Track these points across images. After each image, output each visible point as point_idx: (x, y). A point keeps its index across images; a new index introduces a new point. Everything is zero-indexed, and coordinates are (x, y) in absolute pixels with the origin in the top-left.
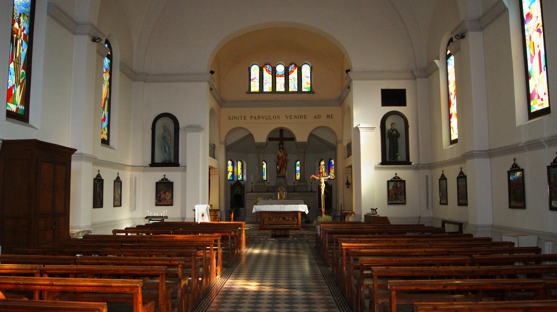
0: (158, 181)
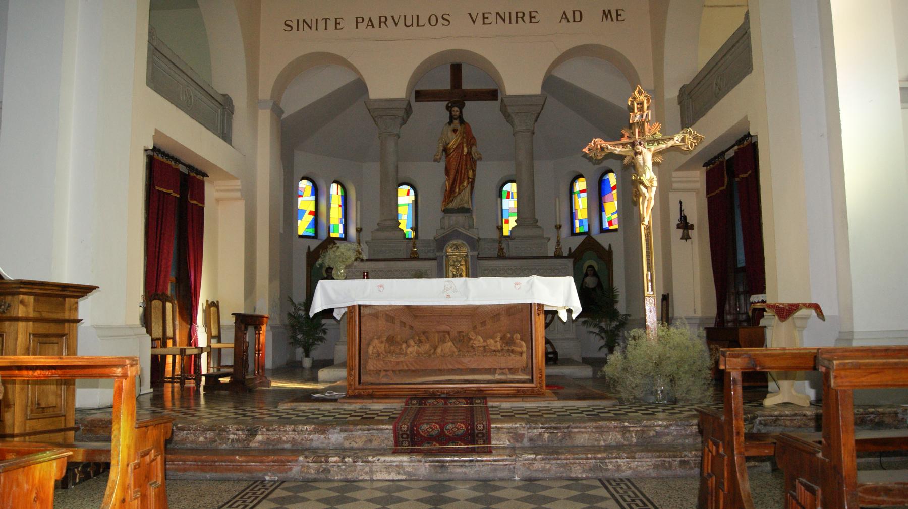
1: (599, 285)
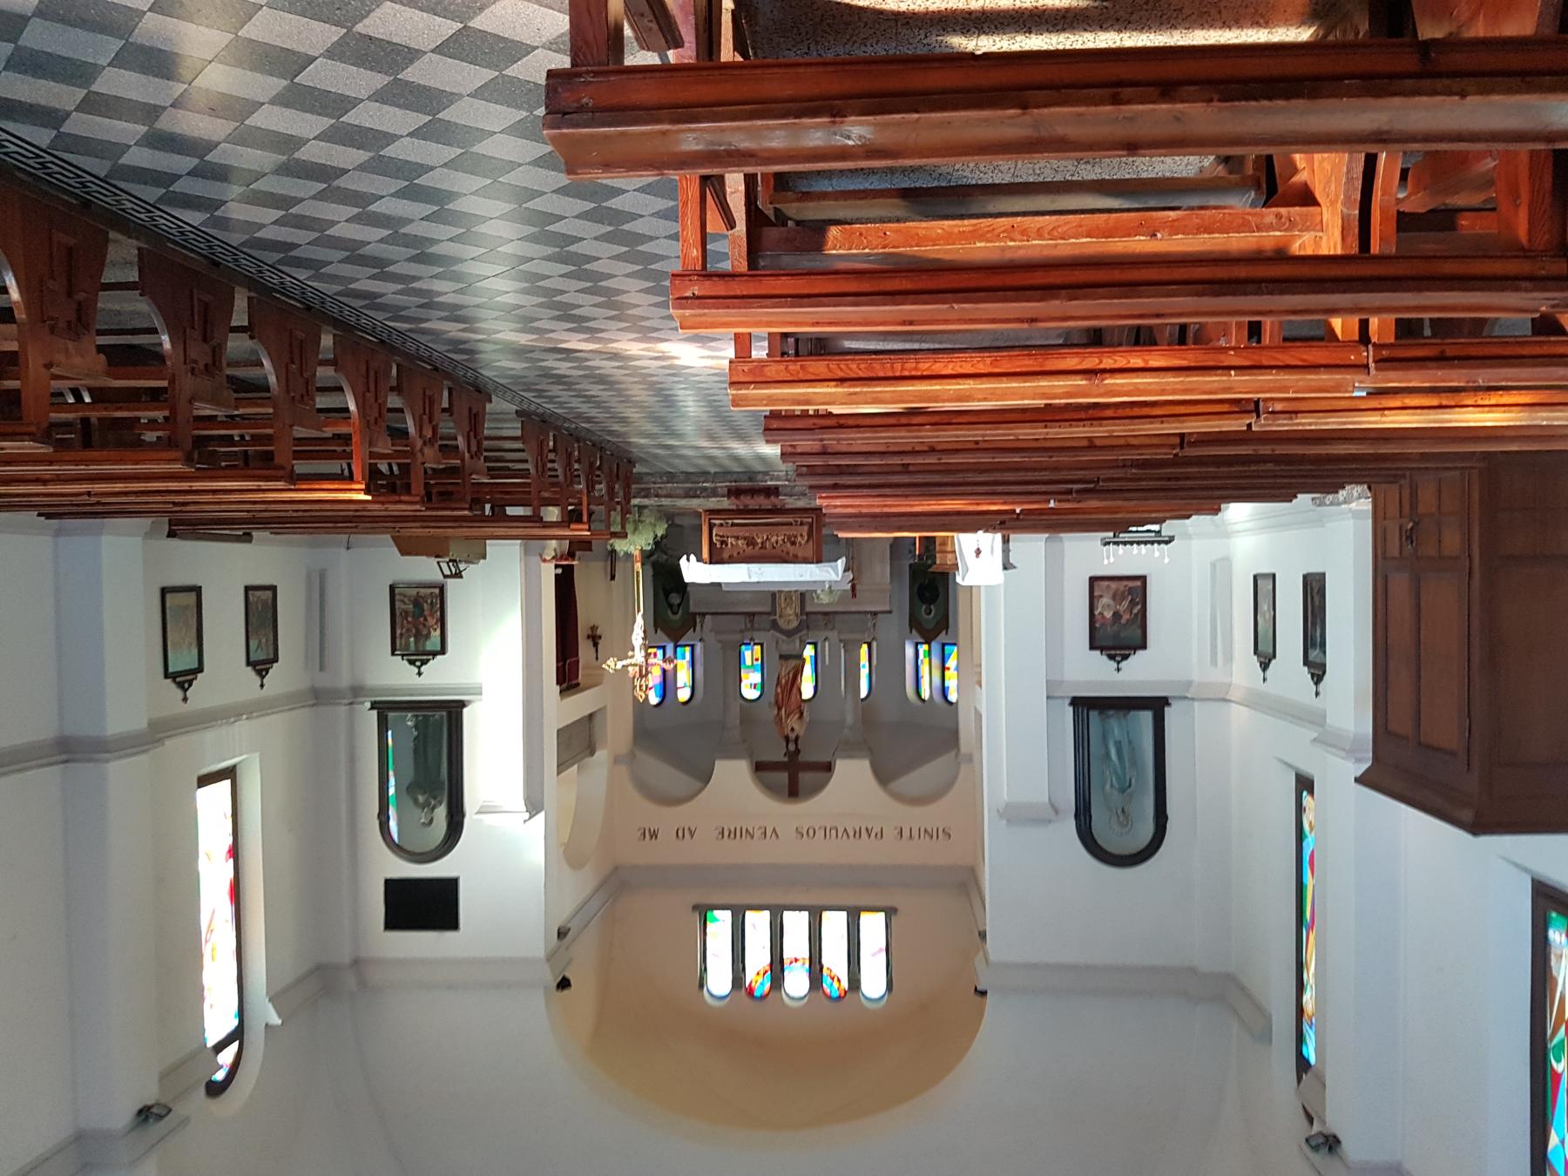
0: (1140, 653)
1: (667, 596)
